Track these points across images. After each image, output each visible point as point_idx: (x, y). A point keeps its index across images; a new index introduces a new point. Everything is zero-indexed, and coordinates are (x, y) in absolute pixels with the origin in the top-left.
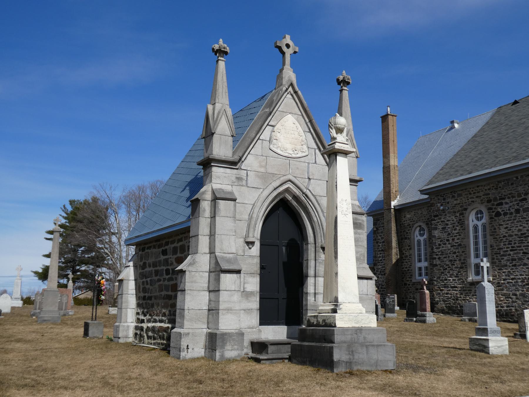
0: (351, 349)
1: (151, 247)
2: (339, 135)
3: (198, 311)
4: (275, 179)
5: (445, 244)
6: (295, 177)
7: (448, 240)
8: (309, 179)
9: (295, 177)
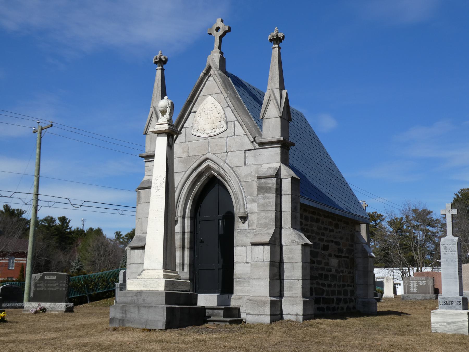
0: (124, 309)
4: (195, 160)
6: (214, 154)
8: (227, 152)
9: (214, 154)
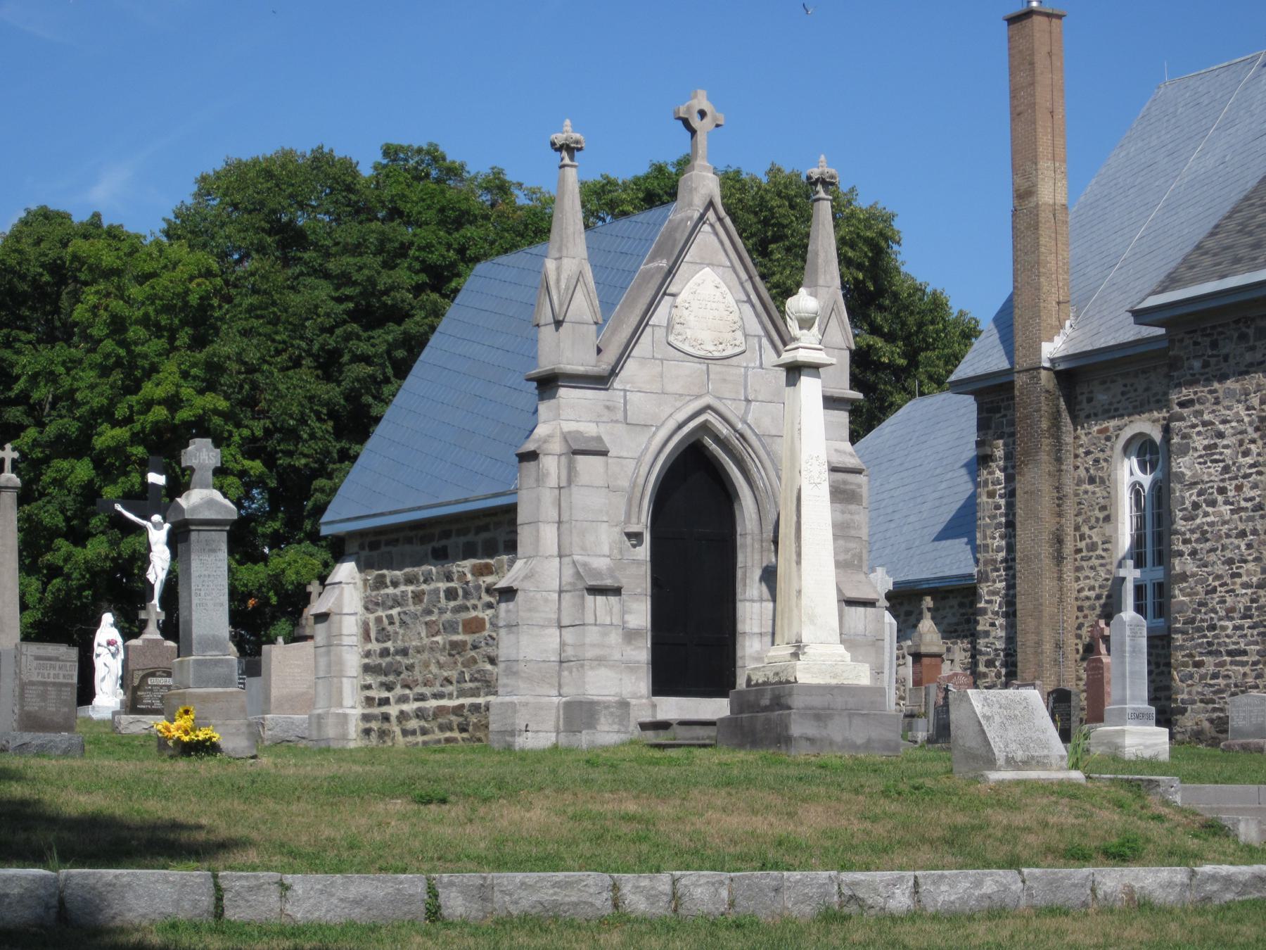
1: (397, 540)
2: (805, 331)
3: (542, 665)
5: (1213, 503)
6: (720, 398)
7: (1222, 491)
8: (748, 401)
